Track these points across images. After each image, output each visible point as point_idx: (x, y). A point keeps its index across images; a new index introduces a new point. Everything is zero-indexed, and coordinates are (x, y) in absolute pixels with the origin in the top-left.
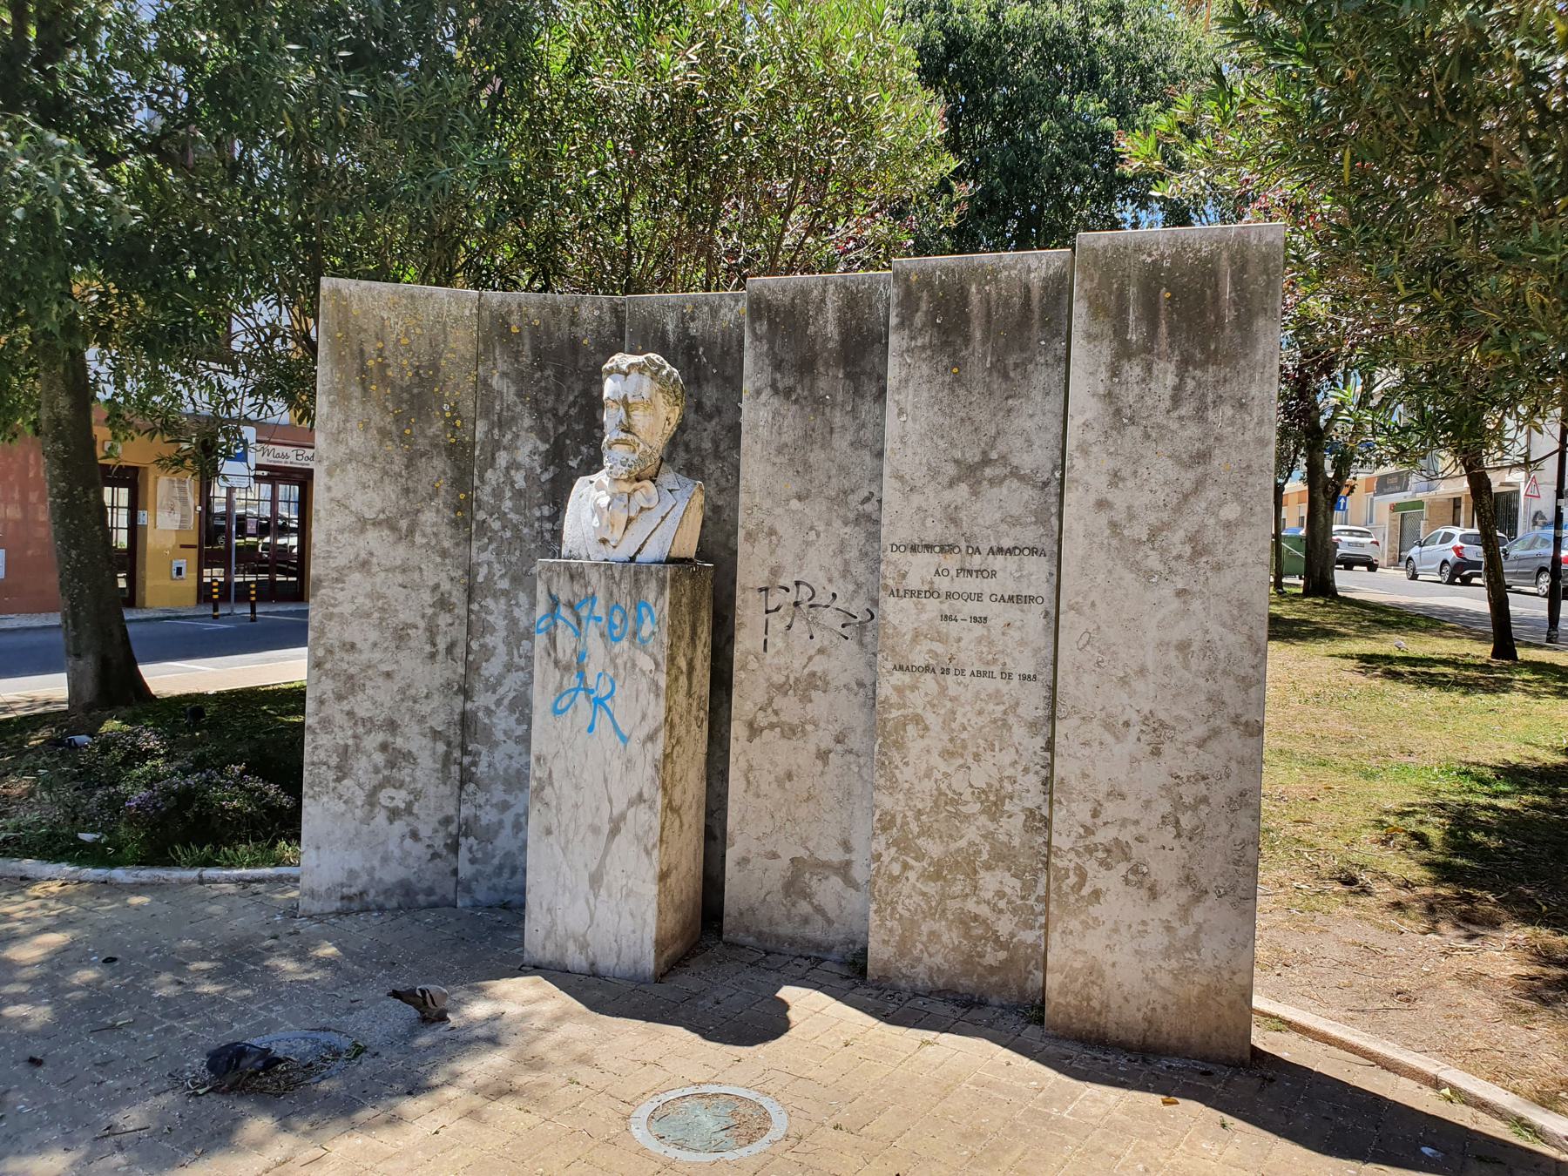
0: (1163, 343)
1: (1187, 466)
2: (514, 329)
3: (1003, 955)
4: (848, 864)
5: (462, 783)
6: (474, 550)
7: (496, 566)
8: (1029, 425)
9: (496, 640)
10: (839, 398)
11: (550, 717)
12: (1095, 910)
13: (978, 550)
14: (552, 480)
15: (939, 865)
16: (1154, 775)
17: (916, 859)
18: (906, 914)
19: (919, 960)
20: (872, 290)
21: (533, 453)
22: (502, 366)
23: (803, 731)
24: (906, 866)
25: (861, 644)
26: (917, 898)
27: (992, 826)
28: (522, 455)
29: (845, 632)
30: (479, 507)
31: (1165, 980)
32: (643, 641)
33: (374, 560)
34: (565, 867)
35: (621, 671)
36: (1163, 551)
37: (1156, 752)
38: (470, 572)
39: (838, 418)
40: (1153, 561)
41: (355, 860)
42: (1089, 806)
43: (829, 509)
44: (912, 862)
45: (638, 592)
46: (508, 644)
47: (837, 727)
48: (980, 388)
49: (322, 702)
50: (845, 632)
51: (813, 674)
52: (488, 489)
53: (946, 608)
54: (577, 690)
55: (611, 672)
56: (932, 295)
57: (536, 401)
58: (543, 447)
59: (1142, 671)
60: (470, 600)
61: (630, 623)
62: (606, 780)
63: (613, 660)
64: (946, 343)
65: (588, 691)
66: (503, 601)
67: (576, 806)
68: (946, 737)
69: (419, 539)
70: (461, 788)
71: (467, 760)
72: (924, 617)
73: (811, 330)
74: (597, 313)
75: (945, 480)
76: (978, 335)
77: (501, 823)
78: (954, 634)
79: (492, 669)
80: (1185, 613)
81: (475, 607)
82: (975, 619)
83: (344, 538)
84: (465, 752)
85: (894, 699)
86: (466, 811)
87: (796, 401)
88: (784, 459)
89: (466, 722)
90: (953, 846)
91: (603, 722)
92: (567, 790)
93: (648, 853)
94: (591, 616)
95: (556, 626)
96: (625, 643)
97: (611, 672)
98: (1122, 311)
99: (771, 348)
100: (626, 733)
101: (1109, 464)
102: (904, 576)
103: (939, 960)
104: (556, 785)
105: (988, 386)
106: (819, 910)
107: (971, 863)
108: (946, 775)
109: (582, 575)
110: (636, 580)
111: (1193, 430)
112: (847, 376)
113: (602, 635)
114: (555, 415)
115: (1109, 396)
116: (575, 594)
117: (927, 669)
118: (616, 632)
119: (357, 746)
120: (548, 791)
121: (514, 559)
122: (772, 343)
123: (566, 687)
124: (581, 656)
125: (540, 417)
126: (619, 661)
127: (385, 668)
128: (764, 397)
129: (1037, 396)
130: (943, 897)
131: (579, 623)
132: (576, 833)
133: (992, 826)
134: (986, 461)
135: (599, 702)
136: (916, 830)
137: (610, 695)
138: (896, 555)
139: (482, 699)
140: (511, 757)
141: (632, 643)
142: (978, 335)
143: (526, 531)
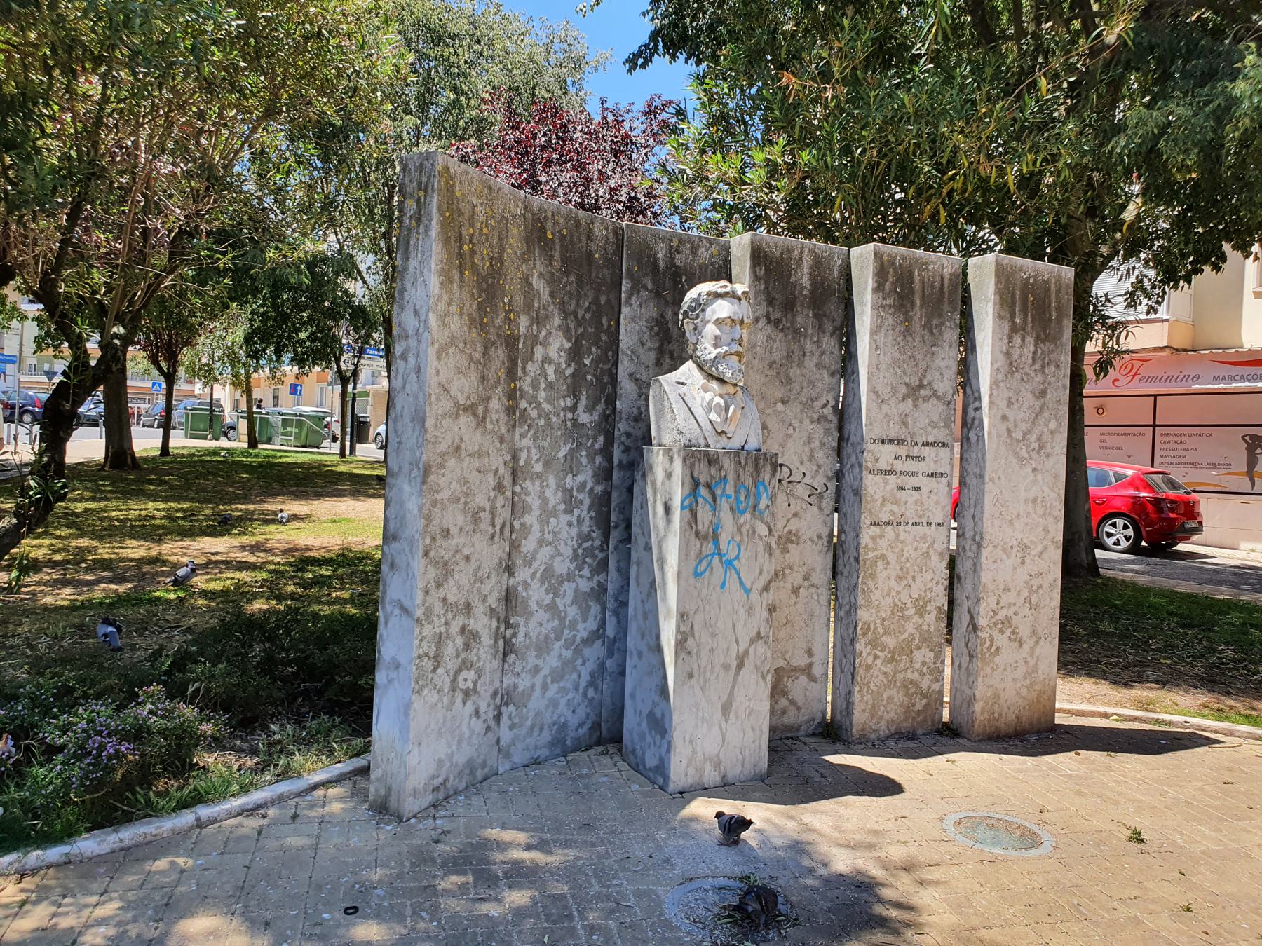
0: (1029, 328)
1: (1038, 398)
2: (549, 235)
3: (924, 702)
4: (811, 665)
5: (505, 655)
6: (517, 436)
7: (533, 451)
8: (942, 364)
9: (531, 519)
10: (810, 331)
11: (692, 580)
12: (997, 660)
13: (916, 444)
14: (573, 375)
15: (893, 652)
16: (1022, 575)
17: (881, 651)
18: (875, 689)
19: (881, 717)
20: (830, 258)
21: (560, 349)
22: (540, 268)
23: (784, 574)
24: (876, 657)
25: (820, 508)
26: (882, 677)
27: (920, 621)
28: (553, 351)
29: (811, 500)
30: (522, 397)
31: (1024, 692)
33: (463, 446)
35: (746, 538)
36: (1028, 446)
37: (1023, 563)
38: (515, 458)
39: (809, 346)
40: (1024, 453)
41: (442, 750)
42: (996, 598)
43: (802, 411)
44: (879, 653)
45: (758, 475)
46: (541, 522)
47: (805, 569)
48: (918, 338)
49: (427, 592)
50: (811, 500)
51: (790, 532)
52: (528, 380)
53: (901, 481)
54: (712, 555)
55: (737, 539)
57: (563, 303)
58: (568, 345)
60: (514, 483)
61: (752, 499)
62: (734, 626)
63: (739, 529)
64: (901, 306)
66: (537, 482)
67: (712, 650)
68: (898, 568)
69: (489, 426)
70: (504, 661)
71: (509, 633)
72: (888, 488)
73: (793, 279)
74: (604, 232)
75: (900, 396)
76: (918, 303)
78: (903, 499)
79: (528, 545)
81: (517, 489)
83: (446, 422)
84: (508, 625)
86: (508, 681)
87: (782, 330)
88: (772, 372)
89: (509, 597)
91: (732, 580)
93: (764, 678)
95: (697, 503)
96: (748, 515)
97: (737, 539)
98: (1013, 305)
99: (766, 288)
100: (748, 586)
101: (1007, 394)
102: (877, 460)
103: (892, 714)
104: (697, 635)
105: (923, 337)
107: (909, 646)
108: (898, 592)
109: (717, 461)
110: (757, 465)
111: (1040, 378)
112: (815, 316)
113: (732, 509)
114: (576, 317)
116: (711, 476)
117: (889, 523)
118: (742, 506)
119: (447, 632)
120: (690, 642)
121: (546, 445)
122: (767, 283)
123: (704, 553)
125: (565, 318)
126: (744, 530)
127: (466, 552)
128: (760, 324)
129: (946, 345)
130: (896, 672)
131: (715, 501)
132: (712, 673)
133: (920, 621)
134: (921, 386)
136: (881, 631)
137: (737, 557)
138: (873, 446)
139: (522, 574)
140: (541, 625)
141: (753, 515)
142: (918, 303)
143: (554, 419)
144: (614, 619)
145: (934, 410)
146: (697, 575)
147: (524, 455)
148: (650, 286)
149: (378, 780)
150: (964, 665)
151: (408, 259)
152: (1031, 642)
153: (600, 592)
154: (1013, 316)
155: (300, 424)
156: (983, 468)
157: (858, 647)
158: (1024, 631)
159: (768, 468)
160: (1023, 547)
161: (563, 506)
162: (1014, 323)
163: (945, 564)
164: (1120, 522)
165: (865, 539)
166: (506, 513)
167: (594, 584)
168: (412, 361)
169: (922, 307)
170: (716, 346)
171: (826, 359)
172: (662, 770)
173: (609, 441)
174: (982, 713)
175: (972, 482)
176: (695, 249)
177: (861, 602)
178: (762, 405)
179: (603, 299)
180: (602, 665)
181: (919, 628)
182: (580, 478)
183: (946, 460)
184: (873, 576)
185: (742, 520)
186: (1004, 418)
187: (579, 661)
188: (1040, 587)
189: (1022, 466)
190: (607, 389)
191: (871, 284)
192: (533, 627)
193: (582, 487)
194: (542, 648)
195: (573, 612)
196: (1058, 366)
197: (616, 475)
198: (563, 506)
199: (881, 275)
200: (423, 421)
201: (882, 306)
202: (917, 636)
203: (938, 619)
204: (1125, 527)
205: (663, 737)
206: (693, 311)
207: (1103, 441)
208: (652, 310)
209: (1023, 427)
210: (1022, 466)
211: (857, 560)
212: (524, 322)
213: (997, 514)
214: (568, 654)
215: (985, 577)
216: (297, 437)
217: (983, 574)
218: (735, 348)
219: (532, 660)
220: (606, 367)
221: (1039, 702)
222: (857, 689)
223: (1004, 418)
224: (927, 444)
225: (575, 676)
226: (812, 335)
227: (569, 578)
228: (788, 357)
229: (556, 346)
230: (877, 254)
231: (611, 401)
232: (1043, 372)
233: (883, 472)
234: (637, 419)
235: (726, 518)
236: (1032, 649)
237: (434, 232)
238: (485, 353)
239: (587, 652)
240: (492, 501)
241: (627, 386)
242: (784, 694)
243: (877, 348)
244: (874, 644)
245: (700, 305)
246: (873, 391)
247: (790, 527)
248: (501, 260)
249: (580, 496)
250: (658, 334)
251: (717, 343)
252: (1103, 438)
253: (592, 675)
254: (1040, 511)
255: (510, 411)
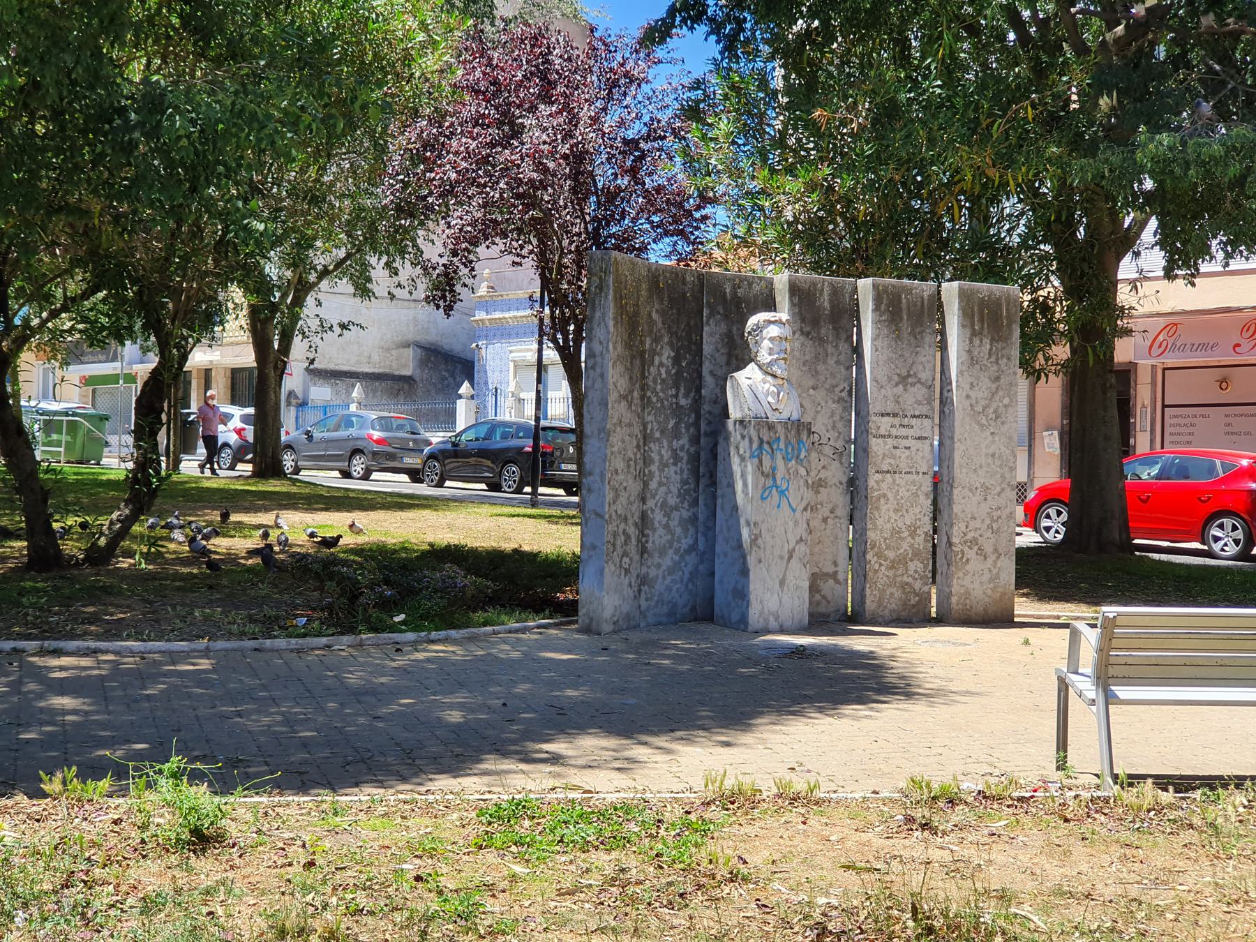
0: (986, 332)
1: (993, 382)
3: (917, 598)
4: (836, 572)
5: (642, 554)
11: (760, 502)
12: (967, 567)
14: (676, 374)
15: (893, 562)
16: (985, 508)
19: (886, 607)
22: (657, 306)
25: (841, 463)
26: (885, 579)
27: (912, 541)
29: (834, 457)
31: (989, 592)
32: (802, 461)
34: (768, 579)
36: (987, 417)
37: (985, 499)
38: (645, 428)
39: (830, 349)
40: (984, 421)
46: (659, 469)
50: (834, 457)
51: (820, 479)
52: (651, 378)
56: (888, 297)
57: (669, 327)
58: (673, 354)
59: (981, 466)
63: (788, 471)
64: (894, 320)
65: (777, 487)
67: (773, 547)
71: (644, 540)
73: (818, 303)
75: (893, 383)
77: (657, 577)
79: (653, 485)
80: (994, 442)
81: (646, 448)
82: (906, 448)
85: (876, 487)
86: (644, 570)
89: (644, 516)
90: (899, 552)
91: (784, 503)
92: (768, 539)
93: (805, 566)
94: (778, 448)
96: (793, 462)
98: (973, 316)
101: (970, 380)
103: (894, 606)
105: (909, 340)
106: (824, 597)
110: (798, 430)
111: (995, 368)
112: (834, 328)
115: (969, 351)
118: (790, 456)
120: (760, 541)
124: (774, 469)
128: (797, 336)
129: (926, 347)
130: (895, 576)
133: (912, 541)
134: (909, 376)
135: (782, 493)
136: (884, 547)
137: (787, 489)
139: (651, 503)
144: (704, 539)
145: (918, 392)
146: (763, 499)
147: (649, 426)
148: (721, 311)
149: (584, 615)
150: (944, 572)
151: (594, 311)
152: (994, 557)
153: (694, 519)
154: (973, 325)
155: (73, 427)
156: (953, 433)
157: (868, 557)
158: (988, 548)
159: (805, 432)
160: (986, 489)
161: (672, 461)
162: (974, 330)
163: (930, 501)
164: (1228, 522)
165: (871, 483)
166: (641, 462)
167: (690, 514)
168: (598, 370)
169: (908, 320)
170: (770, 354)
171: (842, 358)
172: (744, 620)
173: (698, 417)
174: (958, 605)
175: (947, 442)
176: (750, 284)
177: (869, 526)
178: (800, 391)
179: (692, 323)
180: (696, 570)
181: (911, 546)
182: (681, 442)
183: (927, 427)
184: (877, 508)
185: (790, 465)
186: (968, 397)
187: (683, 564)
188: (1000, 517)
189: (982, 431)
190: (696, 383)
191: (871, 306)
192: (657, 538)
193: (682, 448)
194: (662, 553)
195: (678, 530)
196: (1009, 359)
197: (702, 440)
198: (672, 461)
199: (878, 300)
200: (607, 405)
201: (880, 321)
202: (910, 552)
203: (926, 541)
204: (1234, 528)
205: (743, 600)
206: (755, 331)
207: (1229, 425)
208: (723, 328)
209: (983, 403)
210: (982, 431)
211: (866, 497)
212: (648, 341)
213: (965, 465)
214: (677, 558)
215: (956, 509)
216: (69, 446)
217: (954, 506)
218: (782, 356)
219: (656, 559)
220: (695, 367)
221: (1001, 600)
222: (868, 586)
223: (968, 397)
224: (914, 416)
225: (680, 573)
226: (832, 342)
227: (677, 509)
228: (816, 357)
229: (666, 355)
230: (875, 286)
231: (699, 390)
232: (997, 363)
233: (883, 436)
234: (715, 402)
235: (780, 462)
236: (995, 562)
237: (611, 297)
238: (631, 363)
239: (687, 558)
240: (635, 454)
241: (708, 380)
242: (819, 591)
243: (876, 350)
244: (879, 555)
245: (759, 328)
246: (874, 380)
247: (821, 476)
248: (637, 305)
249: (681, 454)
250: (728, 343)
251: (771, 351)
252: (1229, 420)
253: (691, 573)
254: (998, 463)
255: (642, 397)
